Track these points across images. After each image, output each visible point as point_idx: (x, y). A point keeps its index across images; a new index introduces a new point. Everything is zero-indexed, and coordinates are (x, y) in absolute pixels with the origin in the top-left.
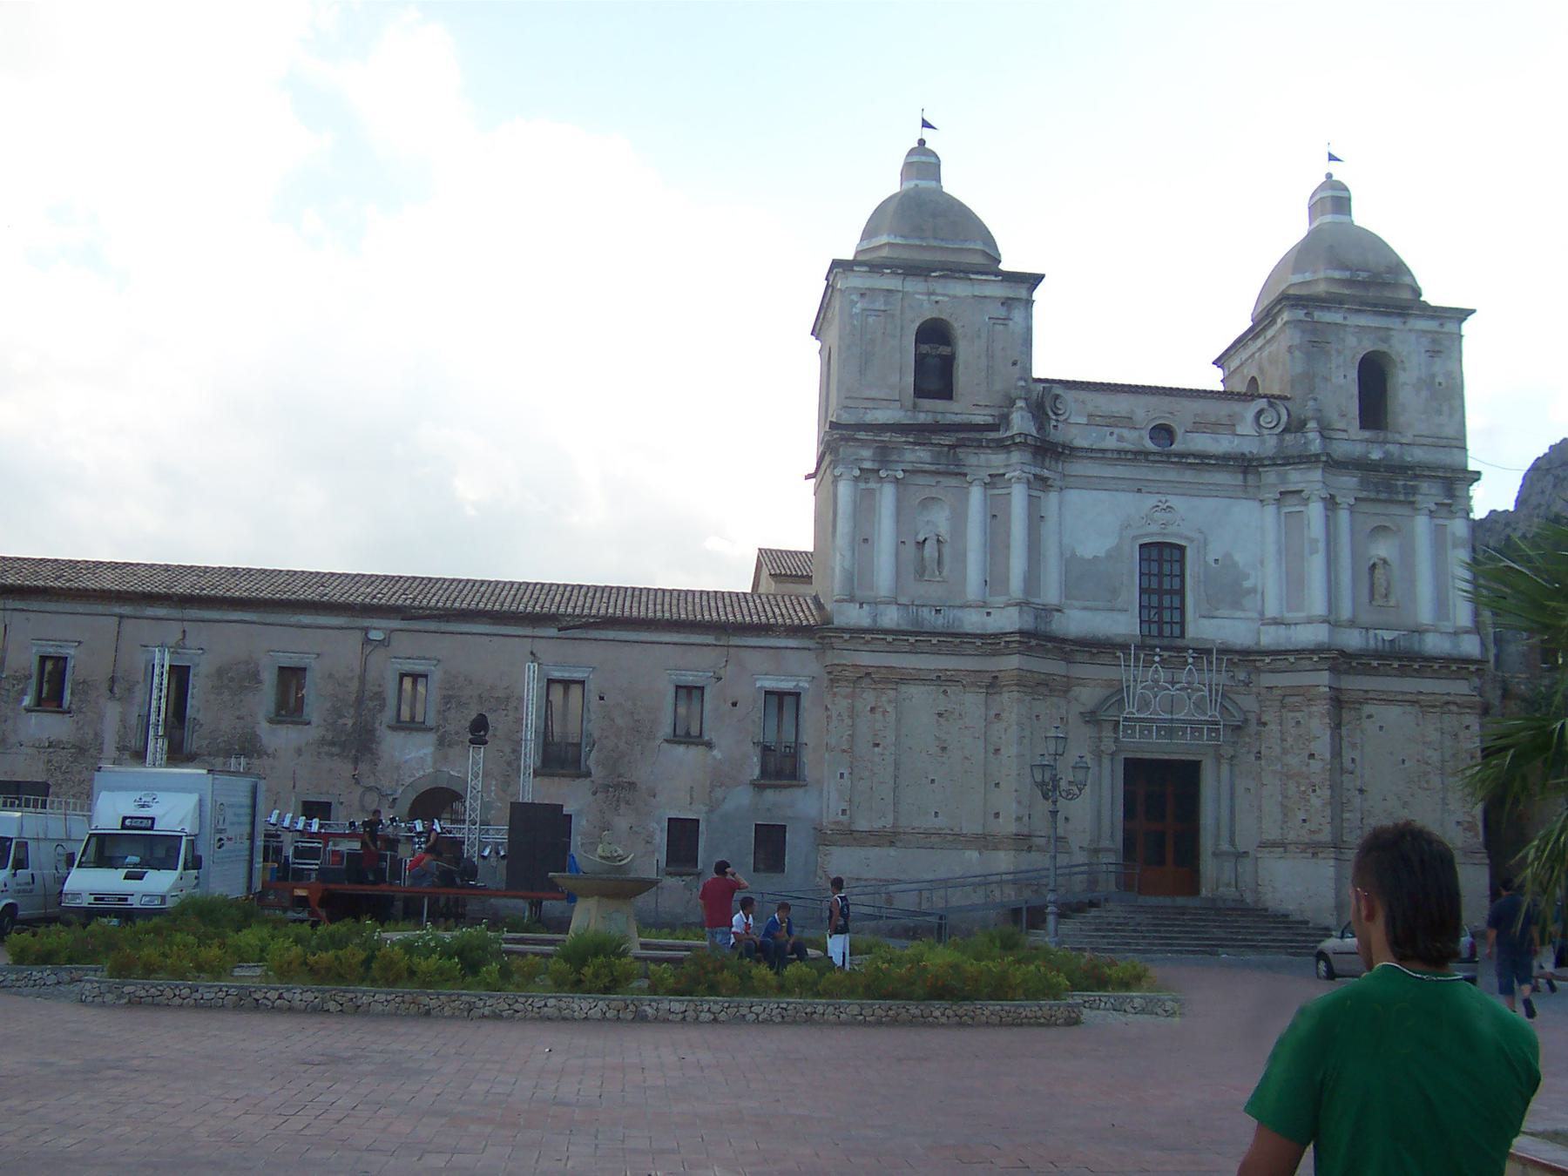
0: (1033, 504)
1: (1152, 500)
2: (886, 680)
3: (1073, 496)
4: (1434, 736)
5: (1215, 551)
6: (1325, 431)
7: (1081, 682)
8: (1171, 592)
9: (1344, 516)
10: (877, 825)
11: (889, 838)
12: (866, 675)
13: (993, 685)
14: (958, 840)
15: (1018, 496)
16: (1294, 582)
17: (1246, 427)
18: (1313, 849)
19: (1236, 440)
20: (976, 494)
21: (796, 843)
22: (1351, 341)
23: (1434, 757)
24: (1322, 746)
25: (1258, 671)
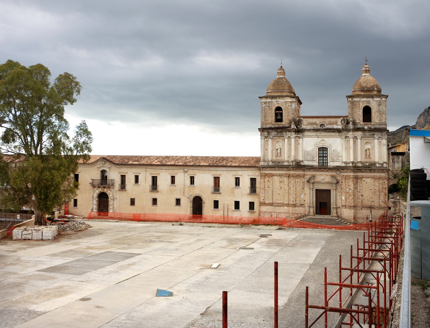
0: (296, 141)
1: (321, 139)
2: (270, 176)
3: (305, 139)
4: (377, 185)
5: (333, 148)
6: (354, 123)
7: (307, 175)
8: (321, 157)
9: (359, 141)
10: (269, 202)
11: (272, 204)
12: (266, 175)
13: (289, 176)
14: (283, 205)
15: (293, 140)
16: (348, 154)
17: (339, 123)
18: (350, 207)
19: (337, 126)
20: (286, 140)
21: (256, 206)
22: (361, 104)
23: (377, 189)
24: (352, 187)
25: (341, 172)
